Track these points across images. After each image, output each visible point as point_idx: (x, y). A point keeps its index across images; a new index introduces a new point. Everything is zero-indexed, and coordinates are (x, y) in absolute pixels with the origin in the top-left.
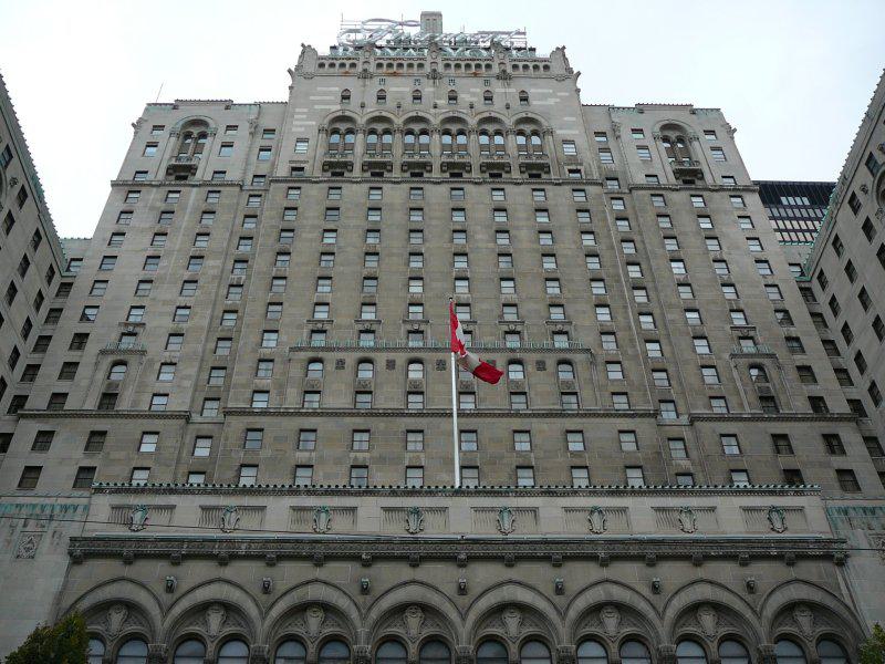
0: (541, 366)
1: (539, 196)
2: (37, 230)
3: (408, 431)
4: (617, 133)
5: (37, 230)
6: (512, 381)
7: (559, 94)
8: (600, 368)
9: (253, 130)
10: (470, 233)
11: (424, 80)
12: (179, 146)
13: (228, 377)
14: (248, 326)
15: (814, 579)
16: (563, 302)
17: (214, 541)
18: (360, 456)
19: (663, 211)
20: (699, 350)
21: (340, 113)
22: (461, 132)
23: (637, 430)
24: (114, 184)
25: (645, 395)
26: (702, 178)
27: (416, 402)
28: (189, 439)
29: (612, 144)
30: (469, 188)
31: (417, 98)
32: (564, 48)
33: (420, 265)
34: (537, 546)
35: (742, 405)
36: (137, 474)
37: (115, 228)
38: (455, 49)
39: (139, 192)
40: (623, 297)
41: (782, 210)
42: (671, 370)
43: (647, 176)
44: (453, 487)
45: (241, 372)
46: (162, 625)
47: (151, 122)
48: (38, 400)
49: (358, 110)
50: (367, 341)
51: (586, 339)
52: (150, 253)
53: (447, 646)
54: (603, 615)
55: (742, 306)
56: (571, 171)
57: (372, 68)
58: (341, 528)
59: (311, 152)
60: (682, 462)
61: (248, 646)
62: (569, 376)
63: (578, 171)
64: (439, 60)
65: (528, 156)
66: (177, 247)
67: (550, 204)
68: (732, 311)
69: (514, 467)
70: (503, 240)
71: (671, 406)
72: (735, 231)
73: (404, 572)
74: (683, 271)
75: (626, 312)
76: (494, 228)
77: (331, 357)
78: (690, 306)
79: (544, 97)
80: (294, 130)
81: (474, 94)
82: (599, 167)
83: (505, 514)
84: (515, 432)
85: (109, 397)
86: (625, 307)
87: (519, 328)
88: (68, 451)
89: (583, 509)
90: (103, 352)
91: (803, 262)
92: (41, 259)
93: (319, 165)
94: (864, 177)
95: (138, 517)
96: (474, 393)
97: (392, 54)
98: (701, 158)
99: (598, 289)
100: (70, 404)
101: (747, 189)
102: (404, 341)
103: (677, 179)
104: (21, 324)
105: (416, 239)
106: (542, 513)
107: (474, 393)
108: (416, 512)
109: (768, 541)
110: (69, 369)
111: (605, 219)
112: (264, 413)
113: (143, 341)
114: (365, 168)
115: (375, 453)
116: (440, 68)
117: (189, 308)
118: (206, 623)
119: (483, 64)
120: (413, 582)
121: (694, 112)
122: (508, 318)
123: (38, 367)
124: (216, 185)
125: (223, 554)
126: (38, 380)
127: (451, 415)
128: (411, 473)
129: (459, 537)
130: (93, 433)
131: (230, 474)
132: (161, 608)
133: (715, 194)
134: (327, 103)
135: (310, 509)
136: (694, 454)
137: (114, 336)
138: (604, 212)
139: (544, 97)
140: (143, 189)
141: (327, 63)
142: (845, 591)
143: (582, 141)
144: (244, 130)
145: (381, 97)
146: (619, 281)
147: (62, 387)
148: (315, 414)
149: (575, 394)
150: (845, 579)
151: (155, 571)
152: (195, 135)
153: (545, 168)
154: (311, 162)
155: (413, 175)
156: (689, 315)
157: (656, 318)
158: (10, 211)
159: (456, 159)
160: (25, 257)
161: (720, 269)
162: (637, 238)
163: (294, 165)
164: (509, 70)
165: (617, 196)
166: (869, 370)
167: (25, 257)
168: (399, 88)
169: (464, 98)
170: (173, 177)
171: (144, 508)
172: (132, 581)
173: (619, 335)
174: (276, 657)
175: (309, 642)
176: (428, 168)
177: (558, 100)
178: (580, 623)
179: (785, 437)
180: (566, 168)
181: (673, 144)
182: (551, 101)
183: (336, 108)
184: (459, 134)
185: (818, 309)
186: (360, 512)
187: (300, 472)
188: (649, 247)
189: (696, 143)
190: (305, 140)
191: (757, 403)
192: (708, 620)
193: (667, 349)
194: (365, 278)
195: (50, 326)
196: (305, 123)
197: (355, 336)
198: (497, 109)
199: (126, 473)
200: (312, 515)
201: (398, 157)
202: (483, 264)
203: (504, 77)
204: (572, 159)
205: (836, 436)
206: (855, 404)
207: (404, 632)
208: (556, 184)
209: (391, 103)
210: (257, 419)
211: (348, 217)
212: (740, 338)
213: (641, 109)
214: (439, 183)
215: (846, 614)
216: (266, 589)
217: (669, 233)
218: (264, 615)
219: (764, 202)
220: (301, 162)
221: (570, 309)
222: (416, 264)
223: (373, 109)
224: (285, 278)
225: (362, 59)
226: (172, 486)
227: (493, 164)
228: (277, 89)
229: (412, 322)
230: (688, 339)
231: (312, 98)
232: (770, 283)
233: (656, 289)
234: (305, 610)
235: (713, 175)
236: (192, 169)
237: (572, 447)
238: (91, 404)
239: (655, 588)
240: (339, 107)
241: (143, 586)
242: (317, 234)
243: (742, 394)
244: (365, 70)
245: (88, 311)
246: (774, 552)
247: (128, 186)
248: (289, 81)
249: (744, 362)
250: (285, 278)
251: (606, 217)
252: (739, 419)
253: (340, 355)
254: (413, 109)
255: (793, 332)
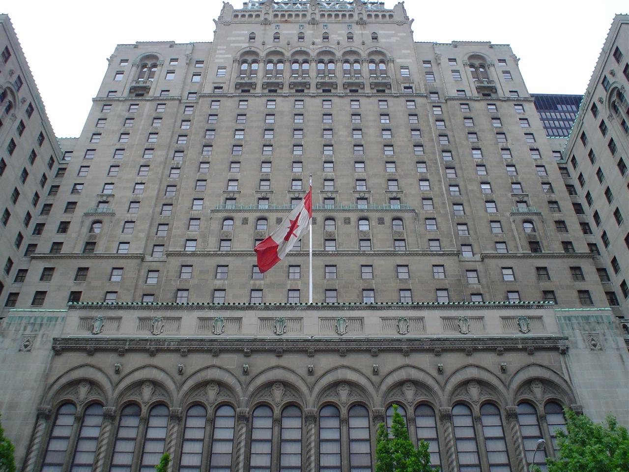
0: (381, 221)
1: (383, 105)
2: (41, 133)
3: (290, 266)
4: (439, 62)
5: (41, 133)
6: (361, 231)
7: (399, 34)
8: (422, 222)
9: (188, 62)
10: (335, 130)
11: (306, 26)
12: (139, 75)
13: (170, 230)
14: (183, 195)
15: (546, 364)
16: (397, 177)
17: (146, 340)
18: (258, 282)
19: (468, 115)
20: (489, 210)
21: (248, 49)
22: (331, 61)
23: (445, 265)
24: (94, 100)
25: (451, 241)
26: (496, 92)
27: (365, 247)
28: (143, 272)
29: (435, 69)
30: (335, 100)
31: (301, 38)
32: (403, 2)
33: (300, 153)
34: (362, 343)
35: (517, 248)
36: (109, 296)
37: (94, 130)
38: (328, 4)
39: (111, 105)
40: (438, 174)
41: (558, 114)
42: (470, 224)
43: (458, 91)
44: (306, 304)
45: (178, 226)
46: (112, 394)
47: (120, 58)
48: (44, 247)
49: (261, 47)
50: (264, 205)
51: (412, 202)
52: (118, 147)
53: (300, 409)
54: (405, 388)
55: (520, 180)
56: (405, 88)
57: (270, 17)
58: (231, 333)
59: (228, 77)
60: (475, 286)
61: (235, 411)
62: (400, 229)
63: (411, 88)
64: (317, 11)
65: (350, 78)
66: (136, 143)
67: (391, 111)
68: (513, 183)
69: (361, 289)
70: (357, 136)
71: (469, 248)
72: (515, 129)
73: (273, 360)
74: (480, 156)
75: (440, 185)
76: (352, 127)
77: (239, 216)
78: (485, 180)
79: (389, 36)
80: (216, 61)
81: (340, 35)
82: (425, 85)
83: (341, 322)
84: (362, 266)
85: (90, 245)
86: (440, 181)
87: (366, 196)
88: (63, 282)
89: (394, 318)
90: (87, 215)
91: (562, 150)
92: (44, 153)
93: (233, 85)
94: (601, 93)
95: (97, 324)
96: (335, 240)
97: (285, 7)
98: (496, 80)
99: (422, 169)
100: (65, 250)
101: (526, 100)
102: (388, 205)
103: (478, 92)
104: (31, 196)
105: (298, 135)
106: (366, 321)
107: (335, 240)
108: (281, 321)
109: (516, 339)
110: (64, 227)
111: (428, 121)
112: (193, 254)
113: (112, 207)
114: (265, 86)
115: (268, 280)
116: (318, 17)
117: (144, 184)
118: (141, 394)
119: (348, 14)
120: (278, 367)
121: (491, 46)
122: (391, 189)
123: (43, 225)
124: (162, 100)
125: (154, 349)
126: (44, 233)
127: (308, 255)
128: (291, 294)
129: (310, 338)
130: (80, 269)
131: (170, 295)
132: (111, 383)
133: (504, 102)
134: (239, 42)
135: (211, 319)
136: (483, 281)
137: (94, 204)
138: (427, 116)
139: (389, 36)
140: (114, 103)
141: (240, 14)
142: (565, 371)
143: (414, 68)
144: (183, 61)
145: (277, 38)
146: (436, 163)
147: (60, 238)
148: (227, 255)
149: (404, 240)
150: (565, 363)
151: (107, 361)
152: (149, 65)
153: (388, 86)
154: (228, 83)
155: (297, 91)
156: (484, 186)
157: (461, 188)
158: (22, 121)
159: (327, 80)
160: (33, 152)
161: (506, 156)
162: (450, 134)
163: (216, 85)
164: (365, 18)
165: (437, 105)
166: (586, 185)
167: (33, 152)
168: (289, 31)
169: (334, 37)
170: (134, 95)
171: (101, 319)
172: (93, 366)
173: (435, 200)
174: (187, 416)
175: (275, 407)
176: (308, 86)
177: (398, 39)
178: (389, 393)
179: (545, 269)
180: (403, 85)
181: (477, 69)
182: (393, 40)
183: (245, 46)
184: (304, 63)
185: (571, 182)
186: (183, 321)
187: (217, 294)
188: (457, 140)
189: (492, 69)
190: (224, 68)
191: (528, 246)
192: (474, 392)
193: (467, 209)
194: (263, 162)
195: (51, 197)
196: (224, 57)
197: (256, 202)
198: (356, 45)
199: (102, 296)
200: (212, 323)
201: (313, 79)
202: (343, 153)
203: (361, 23)
204: (407, 79)
205: (579, 268)
206: (592, 246)
207: (140, 398)
208: (395, 97)
209: (283, 41)
210: (189, 258)
211: (252, 121)
212: (518, 202)
213: (455, 44)
214: (314, 97)
215: (564, 386)
216: (180, 372)
217: (472, 130)
218: (179, 389)
219: (537, 108)
220: (221, 83)
221: (402, 182)
222: (298, 152)
223: (271, 46)
224: (208, 163)
225: (264, 12)
226: (374, 304)
227: (379, 83)
228: (205, 33)
229: (294, 192)
230: (483, 202)
231: (229, 39)
232: (539, 164)
233: (461, 169)
234: (206, 385)
235: (503, 90)
236: (146, 89)
237: (401, 276)
238: (79, 249)
239: (440, 371)
240: (247, 45)
241: (100, 369)
242: (231, 132)
243: (518, 239)
244: (266, 19)
245: (78, 187)
246: (520, 346)
247: (103, 102)
248: (214, 27)
249: (519, 218)
250: (208, 163)
251: (429, 119)
252: (514, 257)
253: (246, 215)
254: (298, 46)
255: (554, 197)
